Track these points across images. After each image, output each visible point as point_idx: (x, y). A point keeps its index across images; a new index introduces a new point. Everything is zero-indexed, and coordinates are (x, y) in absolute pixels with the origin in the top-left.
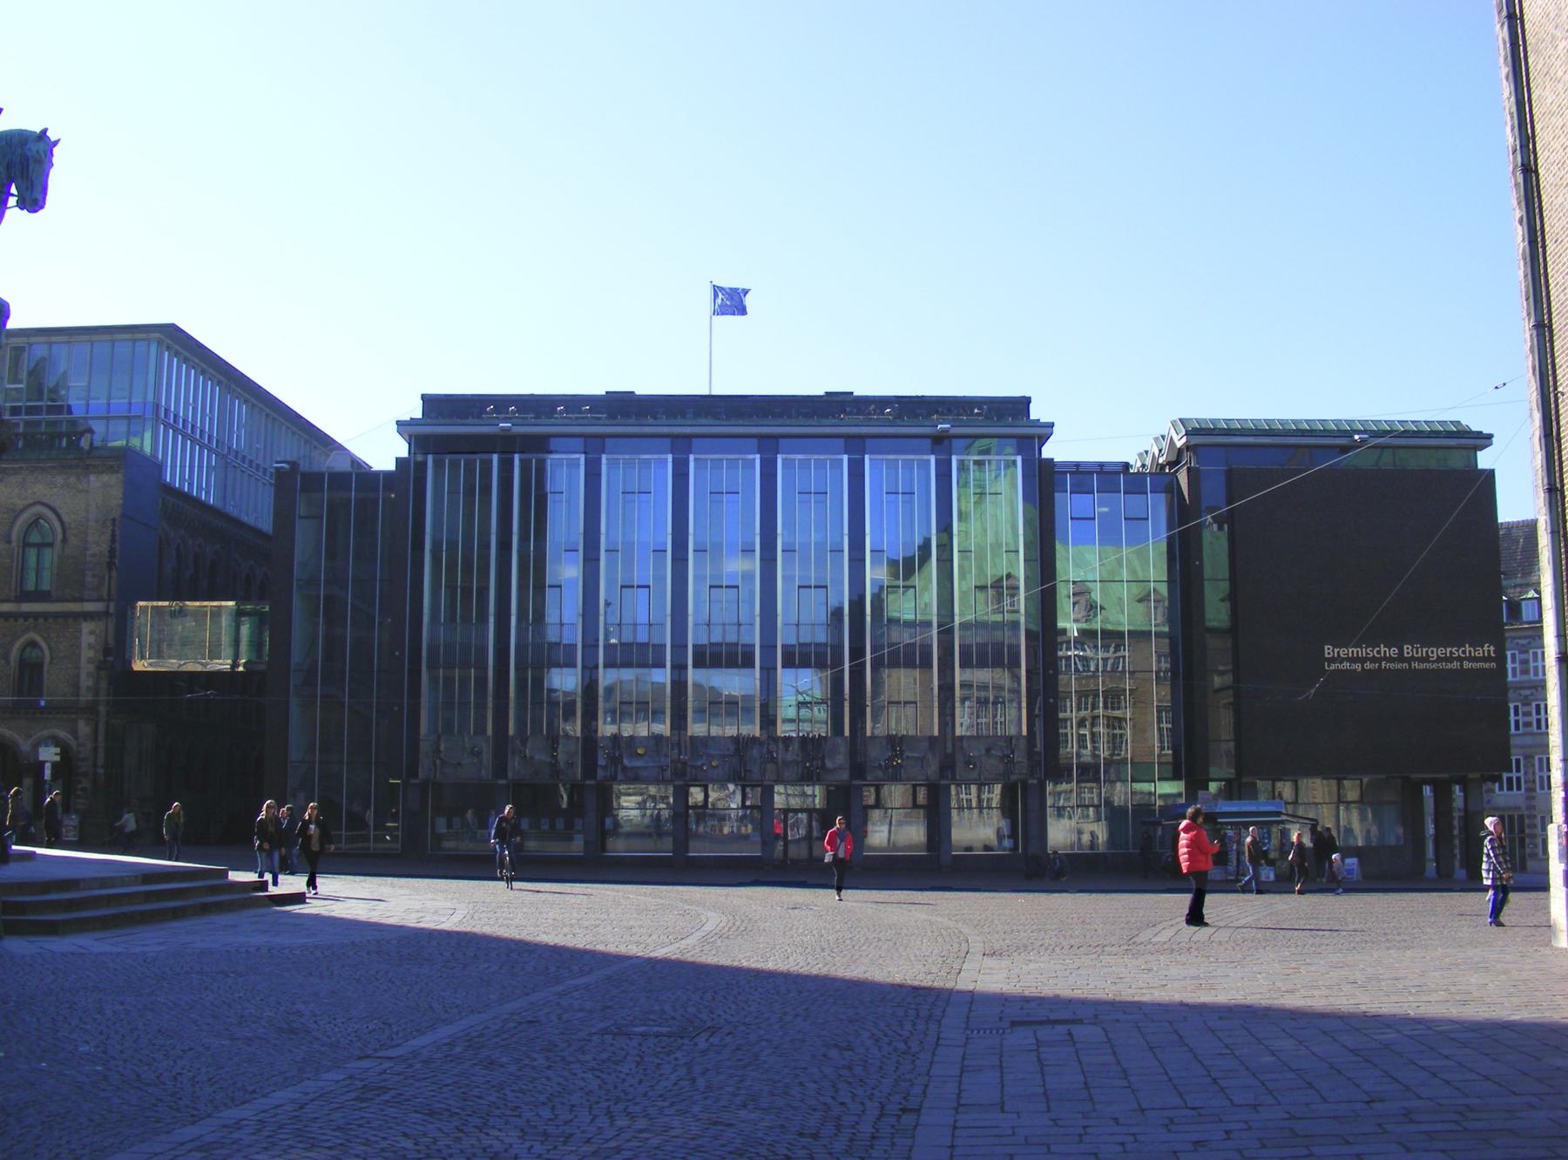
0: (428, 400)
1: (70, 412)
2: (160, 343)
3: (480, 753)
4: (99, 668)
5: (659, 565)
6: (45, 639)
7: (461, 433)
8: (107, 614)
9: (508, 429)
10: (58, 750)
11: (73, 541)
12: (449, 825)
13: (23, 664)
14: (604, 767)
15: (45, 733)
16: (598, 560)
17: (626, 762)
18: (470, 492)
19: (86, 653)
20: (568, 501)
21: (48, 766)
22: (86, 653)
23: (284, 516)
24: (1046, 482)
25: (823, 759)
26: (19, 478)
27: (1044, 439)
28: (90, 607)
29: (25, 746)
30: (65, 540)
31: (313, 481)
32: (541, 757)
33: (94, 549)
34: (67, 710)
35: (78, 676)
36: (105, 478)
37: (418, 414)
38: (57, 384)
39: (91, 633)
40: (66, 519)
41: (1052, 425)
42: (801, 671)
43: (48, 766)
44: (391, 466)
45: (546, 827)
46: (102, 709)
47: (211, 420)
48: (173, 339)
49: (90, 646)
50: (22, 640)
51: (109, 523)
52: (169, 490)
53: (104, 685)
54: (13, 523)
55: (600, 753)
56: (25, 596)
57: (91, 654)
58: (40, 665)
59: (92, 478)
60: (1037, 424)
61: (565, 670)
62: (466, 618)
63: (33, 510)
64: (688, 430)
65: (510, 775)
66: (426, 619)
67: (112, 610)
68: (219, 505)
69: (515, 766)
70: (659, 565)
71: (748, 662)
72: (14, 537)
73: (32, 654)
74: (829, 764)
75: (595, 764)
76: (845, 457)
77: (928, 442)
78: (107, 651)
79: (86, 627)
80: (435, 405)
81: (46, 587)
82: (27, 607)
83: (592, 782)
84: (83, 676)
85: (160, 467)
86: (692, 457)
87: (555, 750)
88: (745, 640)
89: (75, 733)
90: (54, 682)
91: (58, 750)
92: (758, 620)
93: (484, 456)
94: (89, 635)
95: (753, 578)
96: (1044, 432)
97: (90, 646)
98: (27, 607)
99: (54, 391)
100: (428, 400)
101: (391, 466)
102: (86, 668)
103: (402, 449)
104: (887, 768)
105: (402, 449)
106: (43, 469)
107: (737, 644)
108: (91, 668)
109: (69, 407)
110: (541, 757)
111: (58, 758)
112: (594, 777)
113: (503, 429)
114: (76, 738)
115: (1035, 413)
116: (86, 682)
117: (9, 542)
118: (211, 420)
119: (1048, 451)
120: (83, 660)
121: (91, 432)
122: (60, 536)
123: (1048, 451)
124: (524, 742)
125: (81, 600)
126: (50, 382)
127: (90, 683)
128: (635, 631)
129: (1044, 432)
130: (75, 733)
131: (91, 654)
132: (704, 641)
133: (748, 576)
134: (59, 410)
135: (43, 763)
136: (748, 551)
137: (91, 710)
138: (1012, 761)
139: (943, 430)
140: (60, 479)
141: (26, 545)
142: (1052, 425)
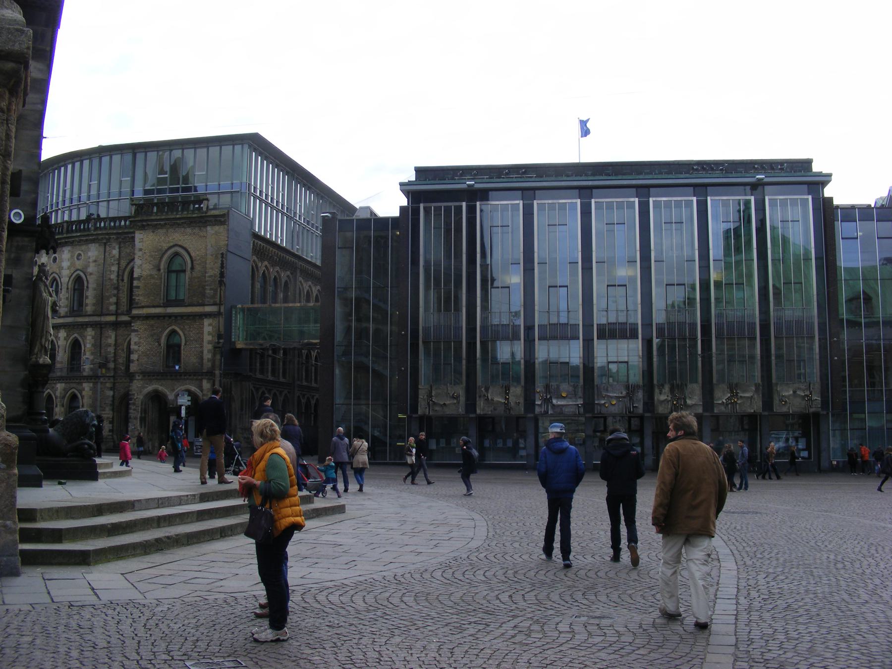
0: (420, 171)
1: (196, 190)
2: (250, 146)
3: (458, 396)
4: (215, 348)
5: (574, 274)
6: (182, 330)
7: (442, 193)
8: (219, 313)
9: (472, 186)
10: (189, 398)
11: (198, 268)
12: (438, 443)
13: (169, 346)
14: (540, 406)
15: (183, 388)
16: (534, 270)
17: (554, 401)
18: (448, 231)
19: (207, 338)
20: (512, 233)
21: (183, 408)
22: (207, 338)
23: (328, 250)
24: (827, 213)
25: (685, 399)
26: (164, 230)
27: (824, 184)
28: (208, 309)
29: (171, 397)
30: (192, 268)
31: (345, 224)
32: (500, 399)
33: (210, 273)
34: (196, 374)
35: (202, 352)
36: (217, 228)
37: (414, 179)
38: (188, 174)
39: (210, 325)
40: (193, 254)
41: (830, 175)
42: (610, 341)
43: (183, 408)
44: (396, 213)
45: (500, 445)
46: (217, 372)
47: (283, 195)
48: (256, 144)
49: (209, 333)
50: (170, 328)
51: (220, 256)
52: (256, 236)
53: (218, 357)
54: (161, 258)
55: (537, 396)
56: (169, 303)
57: (210, 338)
58: (179, 346)
59: (209, 228)
60: (820, 174)
61: (572, 342)
62: (738, 250)
63: (173, 250)
64: (590, 183)
65: (478, 411)
66: (421, 310)
67: (222, 310)
68: (289, 248)
69: (481, 408)
70: (574, 274)
71: (634, 336)
72: (162, 267)
73: (176, 340)
74: (689, 402)
75: (534, 404)
76: (695, 199)
77: (748, 188)
78: (220, 337)
79: (206, 322)
80: (422, 173)
81: (181, 297)
82: (170, 310)
83: (532, 415)
84: (205, 352)
85: (252, 222)
86: (593, 201)
87: (508, 394)
88: (631, 321)
89: (200, 387)
90: (188, 356)
91: (189, 398)
92: (640, 306)
93: (457, 204)
94: (208, 328)
95: (636, 282)
96: (824, 180)
97: (209, 333)
98: (170, 310)
99: (186, 179)
100: (420, 171)
101: (396, 213)
102: (207, 347)
103: (404, 201)
104: (727, 405)
105: (404, 201)
106: (179, 224)
107: (626, 323)
108: (210, 347)
109: (195, 187)
110: (500, 399)
111: (189, 403)
112: (533, 411)
113: (469, 186)
114: (202, 391)
115: (816, 168)
116: (207, 356)
117: (159, 270)
118: (283, 195)
119: (828, 192)
120: (205, 344)
121: (207, 200)
122: (189, 265)
123: (828, 192)
124: (487, 390)
125: (203, 305)
126: (183, 173)
127: (210, 356)
128: (558, 316)
129: (824, 180)
130: (200, 387)
131: (210, 338)
132: (604, 321)
133: (632, 279)
134: (188, 189)
135: (181, 406)
136: (632, 262)
137: (210, 374)
138: (810, 400)
139: (759, 180)
140: (189, 230)
141: (169, 271)
142: (830, 175)
